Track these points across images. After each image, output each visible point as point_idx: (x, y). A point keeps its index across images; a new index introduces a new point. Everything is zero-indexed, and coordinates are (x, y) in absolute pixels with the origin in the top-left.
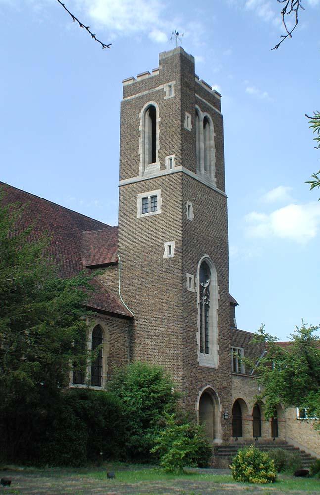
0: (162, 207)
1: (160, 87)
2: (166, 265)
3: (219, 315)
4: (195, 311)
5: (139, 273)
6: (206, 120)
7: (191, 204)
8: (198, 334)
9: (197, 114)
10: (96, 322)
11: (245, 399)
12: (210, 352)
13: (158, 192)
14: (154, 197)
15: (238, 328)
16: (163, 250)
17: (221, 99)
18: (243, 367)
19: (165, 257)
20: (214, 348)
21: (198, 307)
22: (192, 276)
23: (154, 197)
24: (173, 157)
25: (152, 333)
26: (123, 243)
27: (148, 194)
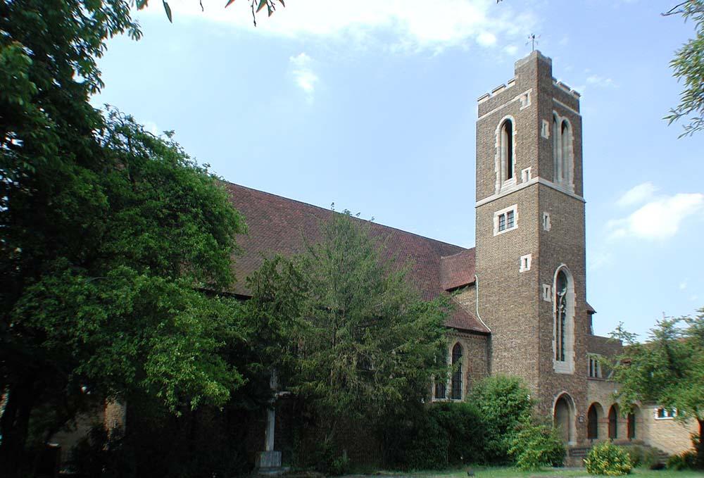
0: (518, 222)
1: (517, 98)
4: (552, 319)
6: (564, 125)
7: (548, 214)
8: (554, 343)
9: (554, 119)
13: (514, 208)
14: (510, 213)
19: (521, 271)
21: (555, 316)
22: (549, 287)
23: (510, 213)
25: (509, 346)
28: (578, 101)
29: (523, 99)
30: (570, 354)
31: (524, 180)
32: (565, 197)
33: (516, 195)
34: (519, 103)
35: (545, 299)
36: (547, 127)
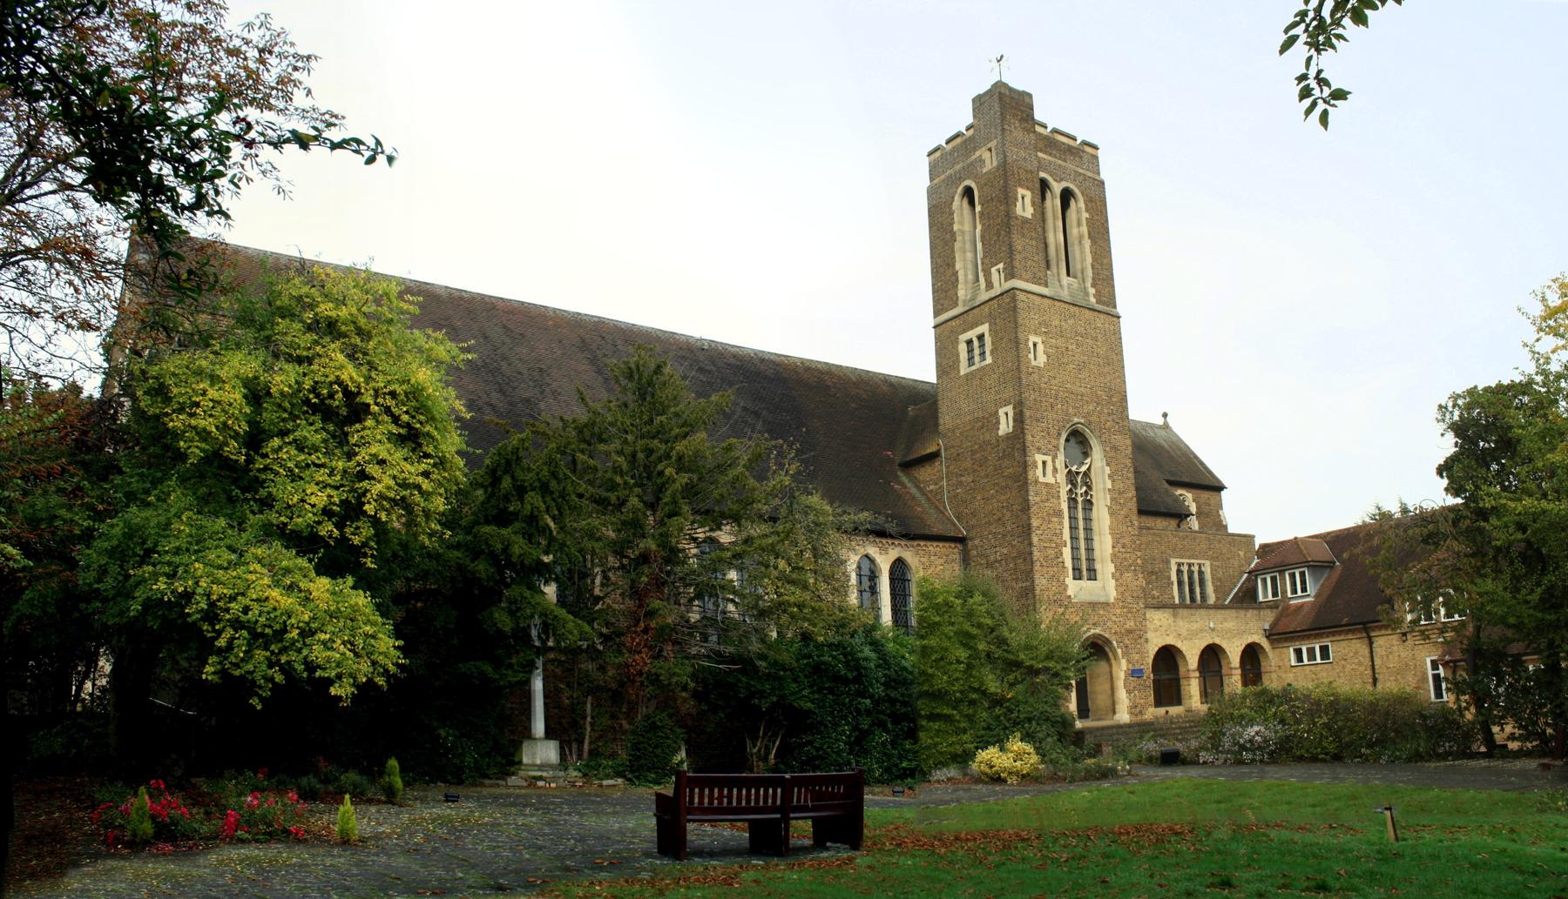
0: (992, 353)
1: (978, 154)
2: (1003, 446)
3: (1112, 513)
4: (1059, 514)
5: (968, 464)
6: (1067, 196)
7: (1038, 340)
8: (1067, 553)
9: (1044, 185)
10: (894, 554)
11: (1179, 645)
12: (1099, 576)
13: (984, 328)
14: (981, 337)
15: (1230, 530)
16: (998, 423)
17: (1100, 153)
18: (1210, 589)
19: (1001, 433)
20: (1106, 568)
21: (1065, 506)
22: (1048, 459)
23: (981, 337)
24: (1001, 266)
25: (992, 558)
26: (946, 419)
27: (972, 334)
28: (1096, 157)
29: (986, 155)
30: (1106, 568)
31: (996, 284)
32: (1073, 309)
33: (986, 309)
34: (981, 161)
35: (1041, 479)
36: (1028, 200)
